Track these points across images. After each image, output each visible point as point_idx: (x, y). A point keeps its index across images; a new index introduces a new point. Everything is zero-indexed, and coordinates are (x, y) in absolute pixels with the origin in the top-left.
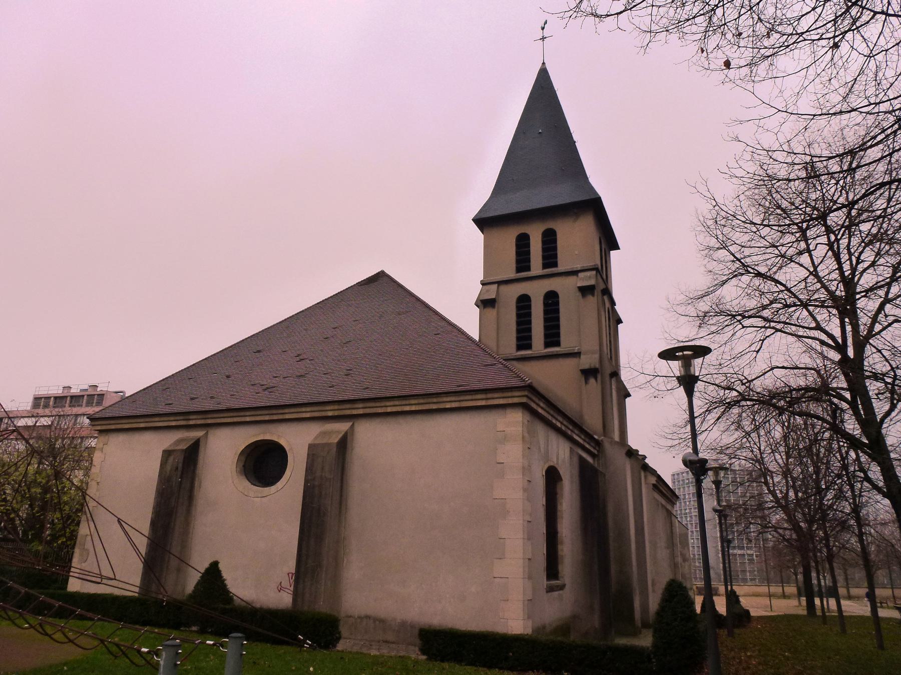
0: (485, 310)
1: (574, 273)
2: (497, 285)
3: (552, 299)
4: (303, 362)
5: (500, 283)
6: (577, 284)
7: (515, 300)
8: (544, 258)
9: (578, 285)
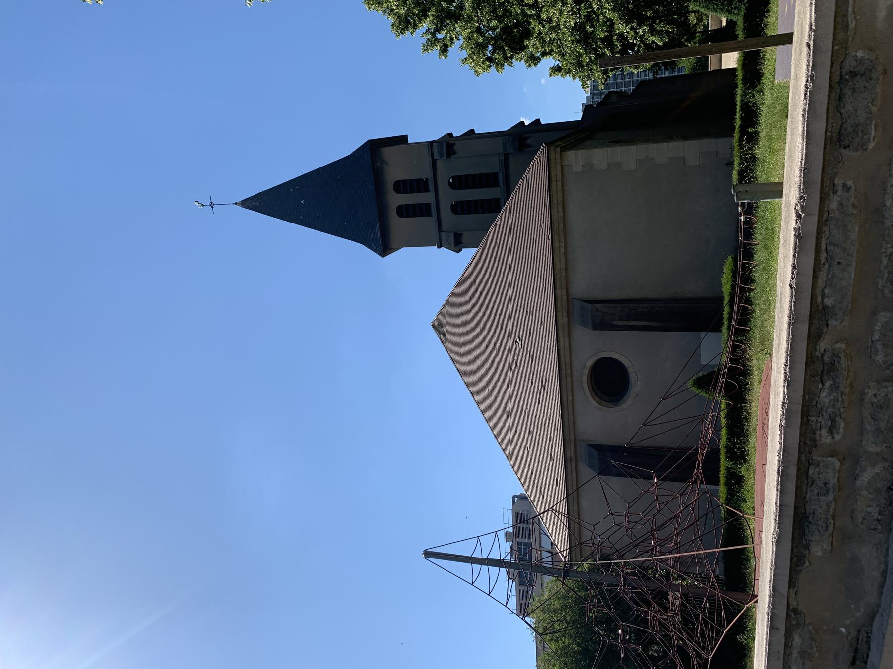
2: (442, 233)
3: (459, 183)
4: (518, 363)
5: (440, 230)
7: (455, 216)
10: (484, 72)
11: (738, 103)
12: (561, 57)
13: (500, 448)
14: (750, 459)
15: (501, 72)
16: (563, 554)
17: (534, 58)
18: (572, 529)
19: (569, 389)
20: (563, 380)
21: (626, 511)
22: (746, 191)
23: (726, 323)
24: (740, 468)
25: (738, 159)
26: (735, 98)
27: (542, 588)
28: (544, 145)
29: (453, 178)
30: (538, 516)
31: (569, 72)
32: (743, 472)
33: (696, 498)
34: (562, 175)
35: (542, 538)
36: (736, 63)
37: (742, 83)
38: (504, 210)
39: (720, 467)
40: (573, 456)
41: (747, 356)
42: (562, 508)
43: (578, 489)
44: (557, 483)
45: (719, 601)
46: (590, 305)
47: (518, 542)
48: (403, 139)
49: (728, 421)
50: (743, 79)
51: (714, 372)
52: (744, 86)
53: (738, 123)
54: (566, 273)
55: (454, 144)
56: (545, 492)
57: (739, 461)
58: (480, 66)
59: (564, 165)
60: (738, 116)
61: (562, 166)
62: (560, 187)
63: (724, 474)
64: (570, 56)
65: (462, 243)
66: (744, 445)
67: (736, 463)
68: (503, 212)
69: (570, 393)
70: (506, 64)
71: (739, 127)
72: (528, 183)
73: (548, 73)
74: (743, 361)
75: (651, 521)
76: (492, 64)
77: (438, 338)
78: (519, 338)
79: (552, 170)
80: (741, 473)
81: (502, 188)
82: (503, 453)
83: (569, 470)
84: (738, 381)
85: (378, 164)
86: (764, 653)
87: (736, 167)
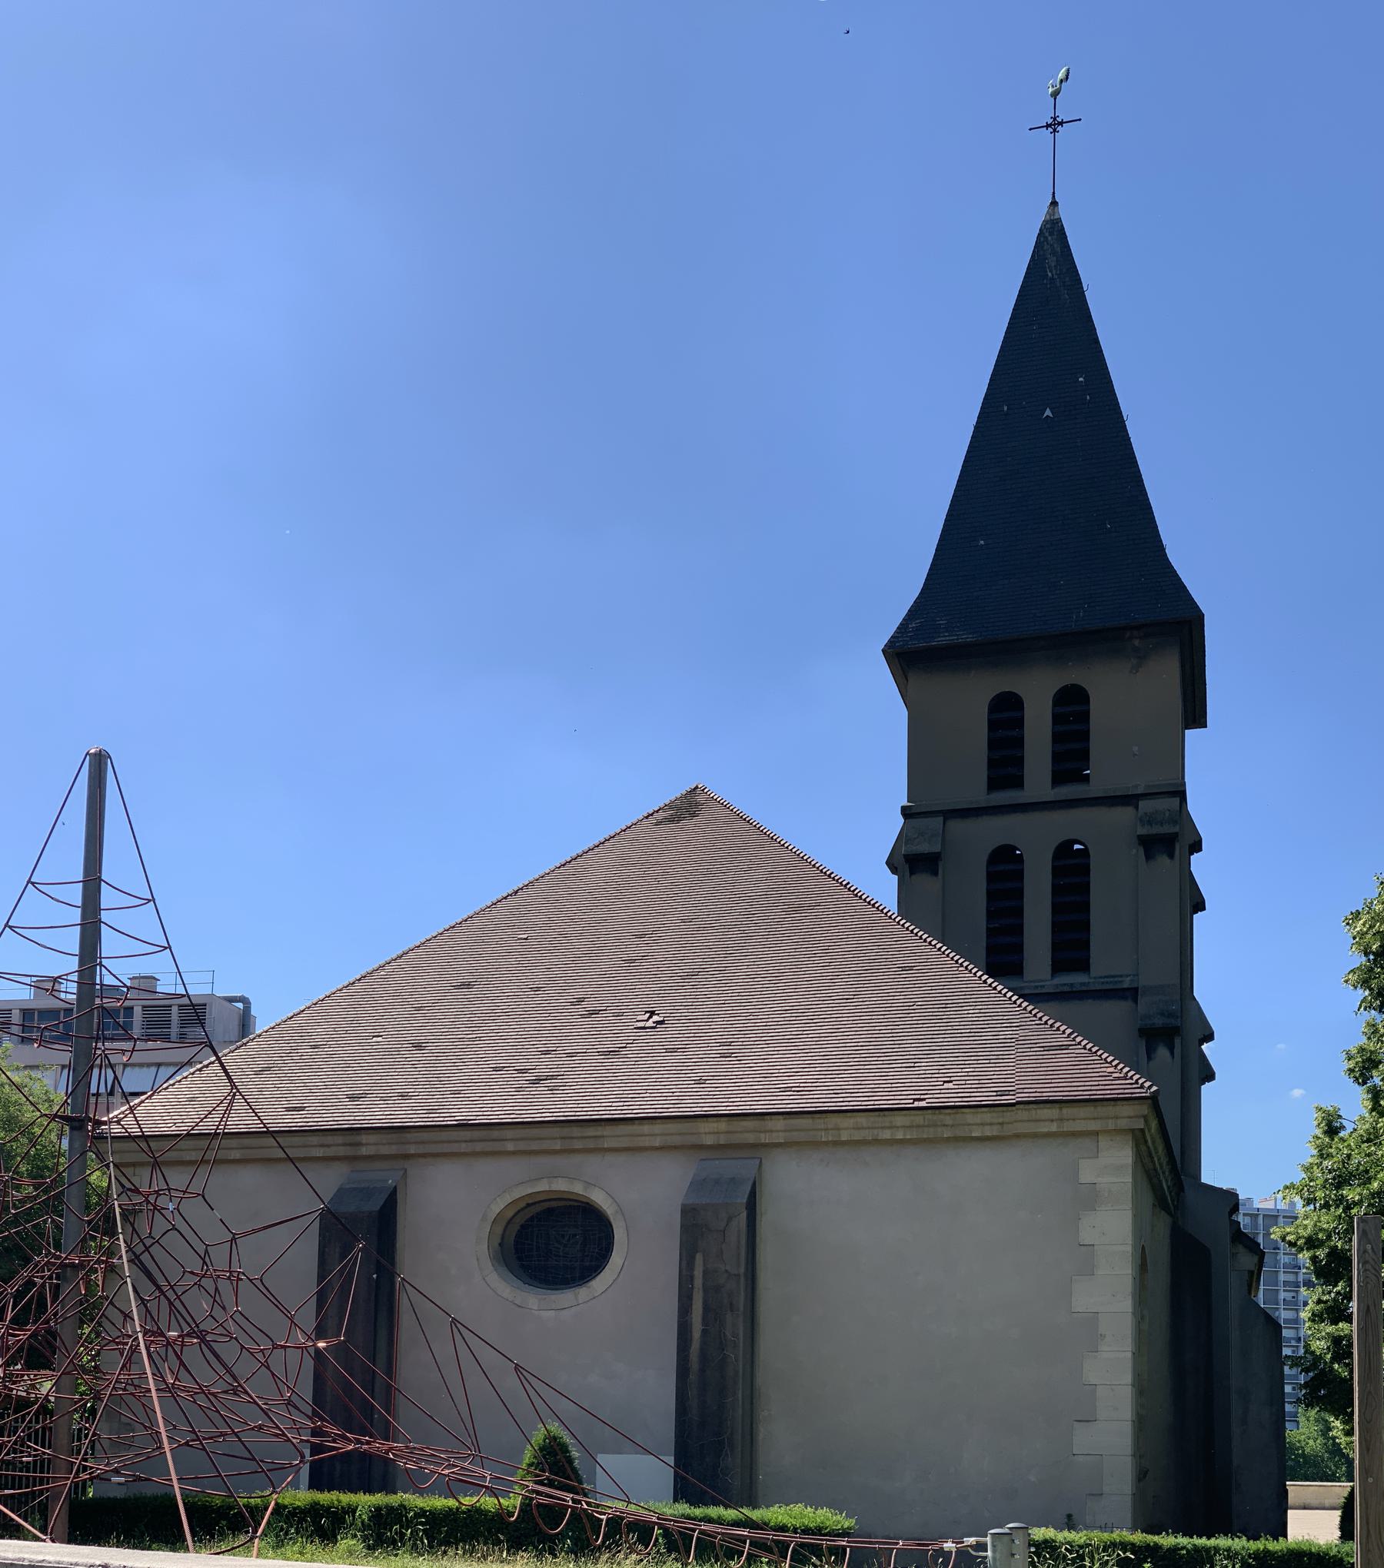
0: (913, 877)
1: (1129, 800)
2: (941, 819)
4: (598, 1017)
6: (1136, 832)
7: (985, 858)
8: (1057, 757)
9: (1138, 833)
10: (1354, 938)
11: (1213, 1542)
12: (1362, 1136)
13: (376, 966)
14: (377, 1558)
15: (1346, 981)
16: (118, 1119)
17: (1368, 1069)
18: (183, 1144)
19: (535, 1146)
20: (555, 1131)
21: (243, 1274)
22: (1013, 1555)
23: (698, 1512)
24: (355, 1536)
25: (1082, 1541)
26: (1226, 1535)
27: (26, 1067)
28: (1154, 1088)
29: (1085, 853)
30: (216, 1054)
31: (1323, 1155)
32: (345, 1543)
33: (289, 1435)
34: (1074, 1134)
35: (145, 1069)
36: (1306, 1538)
37: (1259, 1550)
38: (995, 989)
39: (354, 1491)
40: (364, 1151)
41: (621, 1555)
42: (241, 1120)
43: (291, 1160)
44: (295, 1109)
45: (42, 1481)
46: (745, 1201)
47: (133, 1008)
48: (1196, 716)
49: (464, 1513)
50: (1266, 1552)
51: (581, 1483)
52: (1250, 1556)
53: (1167, 1541)
54: (826, 1143)
55: (1171, 856)
56: (269, 1080)
57: (371, 1535)
58: (1371, 927)
59: (1100, 1137)
60: (1183, 1541)
61: (1097, 1133)
62: (1044, 1128)
63: (339, 1501)
64: (1369, 1155)
65: (912, 873)
66: (409, 1544)
67: (365, 1527)
68: (990, 985)
69: (522, 1146)
70: (1367, 993)
71: (1156, 1544)
72: (1061, 1048)
73: (1327, 1106)
74: (608, 1547)
75: (220, 1330)
76: (1372, 957)
77: (662, 805)
78: (662, 1022)
79: (1088, 1110)
80: (342, 1539)
81: (1048, 983)
82: (363, 973)
83: (329, 1139)
84: (562, 1536)
85: (1136, 642)
86: (10, 1555)
87: (1062, 1536)
